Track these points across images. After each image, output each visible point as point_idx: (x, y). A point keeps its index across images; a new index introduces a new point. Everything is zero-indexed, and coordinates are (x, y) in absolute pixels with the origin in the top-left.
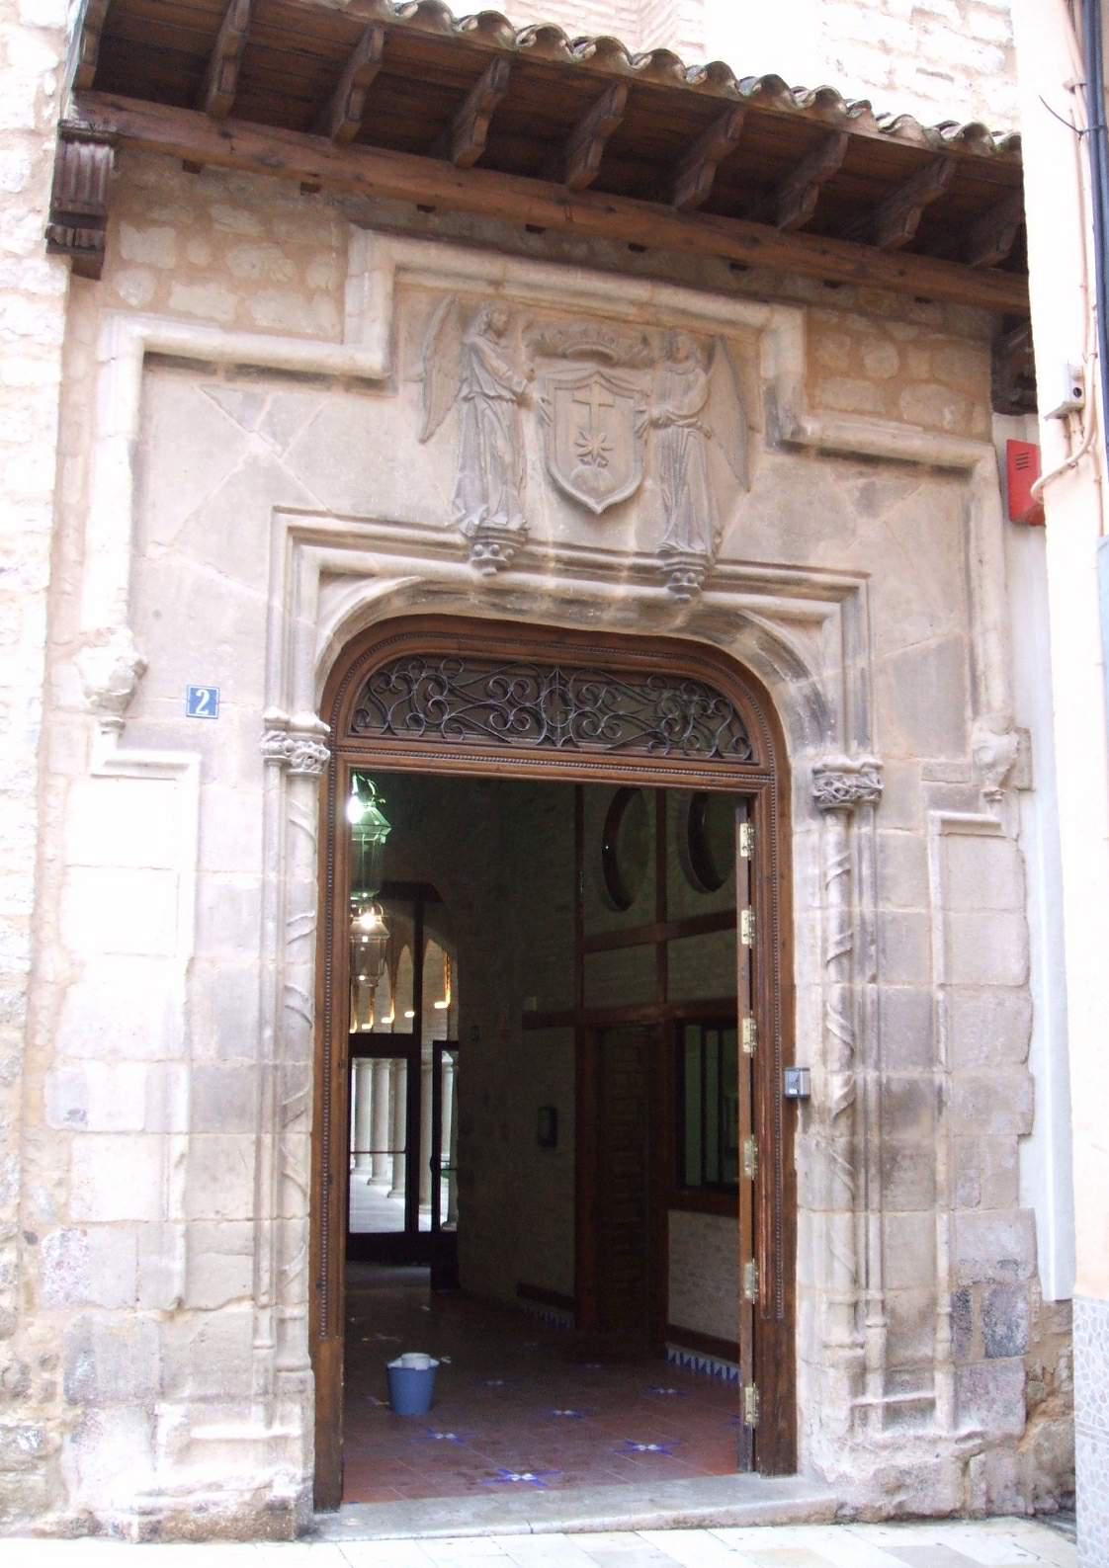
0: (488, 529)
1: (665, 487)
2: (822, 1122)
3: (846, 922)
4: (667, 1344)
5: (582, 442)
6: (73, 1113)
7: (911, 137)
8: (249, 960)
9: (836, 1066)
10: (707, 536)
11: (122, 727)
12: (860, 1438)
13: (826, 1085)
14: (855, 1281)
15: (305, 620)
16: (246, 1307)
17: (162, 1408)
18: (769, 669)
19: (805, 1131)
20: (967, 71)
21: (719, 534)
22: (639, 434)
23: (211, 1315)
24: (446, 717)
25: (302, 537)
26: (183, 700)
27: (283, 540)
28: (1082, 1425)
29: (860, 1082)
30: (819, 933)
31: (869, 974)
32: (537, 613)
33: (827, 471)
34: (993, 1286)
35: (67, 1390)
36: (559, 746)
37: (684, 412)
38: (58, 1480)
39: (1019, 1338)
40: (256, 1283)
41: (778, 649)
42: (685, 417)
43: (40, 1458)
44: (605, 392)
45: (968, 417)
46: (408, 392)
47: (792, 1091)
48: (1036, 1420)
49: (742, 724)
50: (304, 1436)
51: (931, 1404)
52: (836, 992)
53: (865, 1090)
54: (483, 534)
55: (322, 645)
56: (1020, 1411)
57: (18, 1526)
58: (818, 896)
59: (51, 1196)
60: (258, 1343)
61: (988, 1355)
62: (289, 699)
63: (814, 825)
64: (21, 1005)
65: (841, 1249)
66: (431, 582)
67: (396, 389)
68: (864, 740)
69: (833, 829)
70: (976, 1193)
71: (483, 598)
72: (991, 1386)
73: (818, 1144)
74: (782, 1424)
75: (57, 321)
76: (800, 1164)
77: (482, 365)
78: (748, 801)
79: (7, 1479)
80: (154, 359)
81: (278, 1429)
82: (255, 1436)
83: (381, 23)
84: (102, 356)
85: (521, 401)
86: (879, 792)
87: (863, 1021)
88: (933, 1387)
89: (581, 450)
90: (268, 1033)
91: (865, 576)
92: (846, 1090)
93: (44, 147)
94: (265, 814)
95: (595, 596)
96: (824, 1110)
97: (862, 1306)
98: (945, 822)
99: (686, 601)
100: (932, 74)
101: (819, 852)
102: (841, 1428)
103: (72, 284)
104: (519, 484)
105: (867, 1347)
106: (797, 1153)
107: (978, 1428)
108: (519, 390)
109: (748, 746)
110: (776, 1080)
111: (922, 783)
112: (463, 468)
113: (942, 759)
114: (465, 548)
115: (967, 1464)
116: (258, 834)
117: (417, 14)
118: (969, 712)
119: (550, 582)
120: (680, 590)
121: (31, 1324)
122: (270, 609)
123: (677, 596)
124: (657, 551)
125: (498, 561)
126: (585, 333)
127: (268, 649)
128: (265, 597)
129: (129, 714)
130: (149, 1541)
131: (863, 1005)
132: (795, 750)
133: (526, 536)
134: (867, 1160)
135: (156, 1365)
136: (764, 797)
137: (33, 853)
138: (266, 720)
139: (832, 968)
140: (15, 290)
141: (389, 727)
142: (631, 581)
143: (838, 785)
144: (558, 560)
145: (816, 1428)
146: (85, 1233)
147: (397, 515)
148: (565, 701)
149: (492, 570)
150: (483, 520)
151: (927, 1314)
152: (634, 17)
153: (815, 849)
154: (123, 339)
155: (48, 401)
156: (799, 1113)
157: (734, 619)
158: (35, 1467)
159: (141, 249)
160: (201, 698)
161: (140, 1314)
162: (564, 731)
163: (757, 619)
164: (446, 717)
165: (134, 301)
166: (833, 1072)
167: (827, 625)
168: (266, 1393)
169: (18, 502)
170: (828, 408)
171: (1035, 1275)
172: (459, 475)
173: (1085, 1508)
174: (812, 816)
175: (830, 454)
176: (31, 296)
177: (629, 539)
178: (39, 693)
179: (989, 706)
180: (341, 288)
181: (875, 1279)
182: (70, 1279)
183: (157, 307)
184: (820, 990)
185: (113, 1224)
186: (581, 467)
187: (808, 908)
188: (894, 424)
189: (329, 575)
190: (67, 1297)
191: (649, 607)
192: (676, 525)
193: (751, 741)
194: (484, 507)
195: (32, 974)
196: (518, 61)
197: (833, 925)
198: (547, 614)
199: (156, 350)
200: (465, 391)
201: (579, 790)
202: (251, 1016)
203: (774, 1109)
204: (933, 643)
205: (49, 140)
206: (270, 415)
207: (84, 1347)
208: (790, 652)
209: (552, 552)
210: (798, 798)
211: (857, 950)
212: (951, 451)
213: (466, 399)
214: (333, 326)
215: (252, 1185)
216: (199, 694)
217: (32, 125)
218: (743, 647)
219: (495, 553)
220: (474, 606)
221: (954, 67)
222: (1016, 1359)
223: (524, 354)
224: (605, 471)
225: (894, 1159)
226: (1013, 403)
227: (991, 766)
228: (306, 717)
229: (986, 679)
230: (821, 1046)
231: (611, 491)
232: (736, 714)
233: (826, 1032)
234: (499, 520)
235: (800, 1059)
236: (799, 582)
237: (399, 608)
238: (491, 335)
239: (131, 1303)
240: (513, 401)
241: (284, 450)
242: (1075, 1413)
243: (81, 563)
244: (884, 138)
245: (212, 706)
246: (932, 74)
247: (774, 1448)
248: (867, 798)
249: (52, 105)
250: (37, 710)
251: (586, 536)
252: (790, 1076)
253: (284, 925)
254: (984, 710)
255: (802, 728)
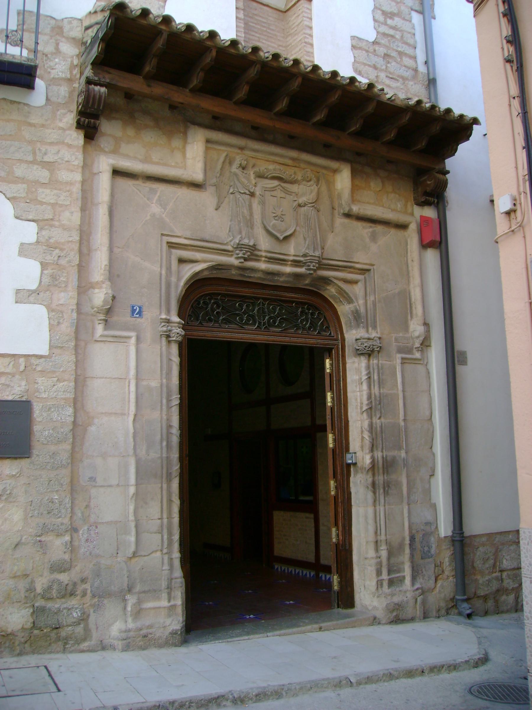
0: (242, 244)
1: (304, 230)
2: (362, 473)
3: (369, 397)
4: (274, 563)
5: (274, 211)
6: (91, 478)
7: (398, 103)
8: (156, 415)
9: (368, 451)
10: (320, 250)
11: (106, 321)
12: (380, 592)
13: (363, 459)
14: (376, 533)
15: (174, 279)
16: (159, 554)
17: (128, 597)
18: (338, 300)
19: (355, 476)
20: (403, 78)
21: (323, 249)
22: (295, 209)
23: (146, 558)
24: (221, 318)
25: (171, 245)
26: (129, 310)
27: (165, 245)
28: (525, 574)
29: (376, 457)
30: (359, 400)
31: (378, 416)
32: (256, 277)
33: (359, 225)
34: (424, 532)
35: (91, 591)
36: (262, 330)
37: (310, 202)
38: (87, 630)
39: (433, 551)
40: (162, 545)
41: (342, 292)
42: (311, 203)
43: (81, 620)
44: (282, 192)
45: (406, 206)
46: (211, 190)
47: (350, 461)
48: (438, 582)
49: (327, 321)
50: (182, 604)
51: (404, 577)
52: (366, 424)
53: (378, 461)
54: (239, 247)
55: (180, 289)
56: (433, 579)
57: (73, 648)
58: (358, 387)
59: (82, 513)
60: (164, 568)
61: (422, 558)
62: (168, 312)
63: (356, 360)
64: (70, 436)
65: (371, 521)
66: (219, 265)
67: (206, 189)
68: (375, 327)
69: (363, 362)
70: (417, 498)
71: (237, 271)
72: (423, 570)
73: (360, 481)
74: (349, 589)
75: (80, 156)
76: (353, 490)
77: (238, 180)
78: (330, 351)
79: (68, 629)
80: (116, 173)
81: (172, 603)
82: (164, 606)
83: (216, 47)
84: (95, 171)
85: (252, 195)
86: (381, 347)
87: (376, 434)
88: (404, 571)
89: (274, 215)
90: (165, 443)
91: (373, 265)
92: (371, 460)
93: (74, 86)
94: (161, 356)
95: (279, 272)
96: (362, 468)
97: (379, 542)
98: (403, 359)
99: (312, 274)
100: (391, 78)
101: (358, 371)
102: (373, 588)
103: (85, 142)
104: (252, 227)
105: (381, 558)
106: (351, 485)
107: (420, 586)
108: (252, 191)
109: (329, 330)
110: (343, 457)
111: (394, 344)
112: (231, 221)
113: (401, 335)
114: (232, 252)
115: (416, 599)
116: (159, 365)
117: (229, 45)
118: (409, 317)
119: (263, 266)
120: (310, 269)
121: (76, 566)
122: (161, 274)
123: (308, 272)
124: (302, 254)
125: (245, 257)
126: (274, 170)
127: (160, 290)
128: (159, 269)
129: (108, 316)
130: (126, 651)
131: (376, 428)
132: (347, 331)
133: (255, 248)
134: (379, 486)
135: (126, 579)
136: (334, 349)
137: (73, 372)
138: (161, 319)
139: (365, 415)
140: (63, 143)
141: (200, 322)
142: (292, 265)
143: (366, 345)
144: (266, 257)
145: (363, 589)
146: (97, 527)
147: (208, 238)
148: (264, 312)
149: (243, 261)
150: (240, 241)
151: (401, 546)
152: (284, 49)
153: (356, 370)
154: (104, 164)
155: (77, 189)
156: (352, 469)
157: (326, 281)
158: (80, 624)
159: (109, 128)
160: (136, 309)
161: (119, 559)
162: (264, 324)
163: (335, 281)
164: (221, 318)
165: (107, 150)
166: (366, 454)
167: (359, 284)
168: (168, 588)
169: (65, 229)
170: (359, 201)
171: (437, 527)
172: (229, 223)
173: (527, 604)
174: (355, 356)
175: (360, 218)
176: (70, 146)
177: (292, 250)
178: (75, 307)
179: (417, 315)
180: (184, 147)
181: (383, 531)
182: (92, 547)
183: (115, 151)
184: (360, 422)
185: (107, 523)
186: (275, 221)
187: (354, 392)
188: (381, 208)
189: (181, 261)
190: (90, 554)
191: (297, 276)
192: (308, 245)
193: (331, 328)
194: (240, 236)
195: (74, 423)
196: (264, 64)
197: (365, 397)
198: (260, 278)
199: (117, 169)
200: (231, 191)
201: (267, 346)
202: (158, 437)
203: (342, 469)
204: (396, 291)
205: (75, 83)
206: (159, 197)
207: (97, 574)
208: (347, 294)
209: (264, 254)
210: (349, 350)
211: (373, 407)
212: (402, 218)
213: (232, 193)
214: (182, 163)
215: (160, 505)
216: (135, 308)
217: (69, 76)
218: (330, 292)
219: (244, 254)
220: (234, 274)
221: (398, 76)
222: (431, 559)
223: (252, 176)
224: (283, 223)
225: (389, 486)
226: (422, 202)
227: (418, 337)
228: (176, 319)
229: (415, 305)
230: (360, 443)
231: (286, 231)
232: (325, 318)
233: (363, 438)
234: (246, 241)
235: (351, 450)
236: (350, 267)
237: (206, 274)
238: (241, 169)
239: (115, 555)
240: (249, 195)
241: (165, 211)
242: (522, 570)
243: (89, 255)
244: (389, 102)
245: (140, 313)
246: (391, 78)
247: (346, 598)
248: (376, 349)
249: (77, 69)
250: (75, 315)
251: (278, 248)
252: (348, 456)
253: (169, 401)
254: (414, 316)
255: (351, 323)
